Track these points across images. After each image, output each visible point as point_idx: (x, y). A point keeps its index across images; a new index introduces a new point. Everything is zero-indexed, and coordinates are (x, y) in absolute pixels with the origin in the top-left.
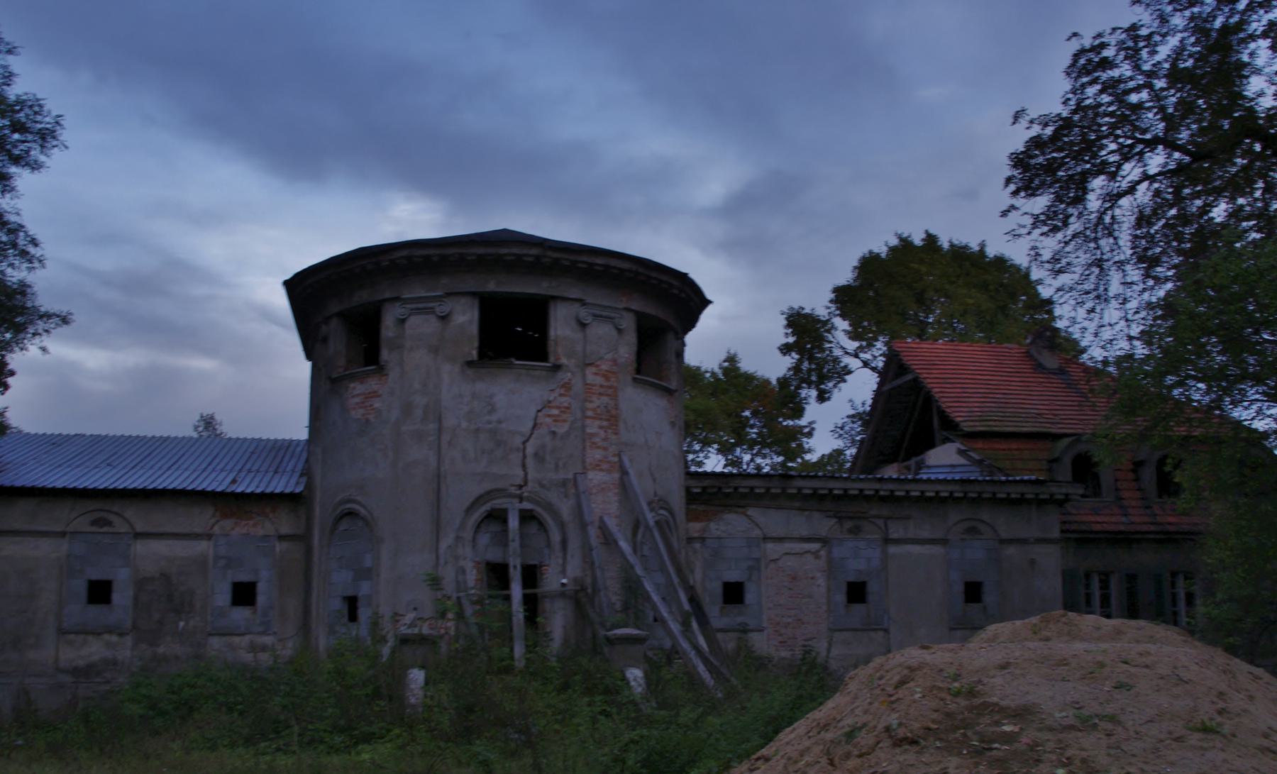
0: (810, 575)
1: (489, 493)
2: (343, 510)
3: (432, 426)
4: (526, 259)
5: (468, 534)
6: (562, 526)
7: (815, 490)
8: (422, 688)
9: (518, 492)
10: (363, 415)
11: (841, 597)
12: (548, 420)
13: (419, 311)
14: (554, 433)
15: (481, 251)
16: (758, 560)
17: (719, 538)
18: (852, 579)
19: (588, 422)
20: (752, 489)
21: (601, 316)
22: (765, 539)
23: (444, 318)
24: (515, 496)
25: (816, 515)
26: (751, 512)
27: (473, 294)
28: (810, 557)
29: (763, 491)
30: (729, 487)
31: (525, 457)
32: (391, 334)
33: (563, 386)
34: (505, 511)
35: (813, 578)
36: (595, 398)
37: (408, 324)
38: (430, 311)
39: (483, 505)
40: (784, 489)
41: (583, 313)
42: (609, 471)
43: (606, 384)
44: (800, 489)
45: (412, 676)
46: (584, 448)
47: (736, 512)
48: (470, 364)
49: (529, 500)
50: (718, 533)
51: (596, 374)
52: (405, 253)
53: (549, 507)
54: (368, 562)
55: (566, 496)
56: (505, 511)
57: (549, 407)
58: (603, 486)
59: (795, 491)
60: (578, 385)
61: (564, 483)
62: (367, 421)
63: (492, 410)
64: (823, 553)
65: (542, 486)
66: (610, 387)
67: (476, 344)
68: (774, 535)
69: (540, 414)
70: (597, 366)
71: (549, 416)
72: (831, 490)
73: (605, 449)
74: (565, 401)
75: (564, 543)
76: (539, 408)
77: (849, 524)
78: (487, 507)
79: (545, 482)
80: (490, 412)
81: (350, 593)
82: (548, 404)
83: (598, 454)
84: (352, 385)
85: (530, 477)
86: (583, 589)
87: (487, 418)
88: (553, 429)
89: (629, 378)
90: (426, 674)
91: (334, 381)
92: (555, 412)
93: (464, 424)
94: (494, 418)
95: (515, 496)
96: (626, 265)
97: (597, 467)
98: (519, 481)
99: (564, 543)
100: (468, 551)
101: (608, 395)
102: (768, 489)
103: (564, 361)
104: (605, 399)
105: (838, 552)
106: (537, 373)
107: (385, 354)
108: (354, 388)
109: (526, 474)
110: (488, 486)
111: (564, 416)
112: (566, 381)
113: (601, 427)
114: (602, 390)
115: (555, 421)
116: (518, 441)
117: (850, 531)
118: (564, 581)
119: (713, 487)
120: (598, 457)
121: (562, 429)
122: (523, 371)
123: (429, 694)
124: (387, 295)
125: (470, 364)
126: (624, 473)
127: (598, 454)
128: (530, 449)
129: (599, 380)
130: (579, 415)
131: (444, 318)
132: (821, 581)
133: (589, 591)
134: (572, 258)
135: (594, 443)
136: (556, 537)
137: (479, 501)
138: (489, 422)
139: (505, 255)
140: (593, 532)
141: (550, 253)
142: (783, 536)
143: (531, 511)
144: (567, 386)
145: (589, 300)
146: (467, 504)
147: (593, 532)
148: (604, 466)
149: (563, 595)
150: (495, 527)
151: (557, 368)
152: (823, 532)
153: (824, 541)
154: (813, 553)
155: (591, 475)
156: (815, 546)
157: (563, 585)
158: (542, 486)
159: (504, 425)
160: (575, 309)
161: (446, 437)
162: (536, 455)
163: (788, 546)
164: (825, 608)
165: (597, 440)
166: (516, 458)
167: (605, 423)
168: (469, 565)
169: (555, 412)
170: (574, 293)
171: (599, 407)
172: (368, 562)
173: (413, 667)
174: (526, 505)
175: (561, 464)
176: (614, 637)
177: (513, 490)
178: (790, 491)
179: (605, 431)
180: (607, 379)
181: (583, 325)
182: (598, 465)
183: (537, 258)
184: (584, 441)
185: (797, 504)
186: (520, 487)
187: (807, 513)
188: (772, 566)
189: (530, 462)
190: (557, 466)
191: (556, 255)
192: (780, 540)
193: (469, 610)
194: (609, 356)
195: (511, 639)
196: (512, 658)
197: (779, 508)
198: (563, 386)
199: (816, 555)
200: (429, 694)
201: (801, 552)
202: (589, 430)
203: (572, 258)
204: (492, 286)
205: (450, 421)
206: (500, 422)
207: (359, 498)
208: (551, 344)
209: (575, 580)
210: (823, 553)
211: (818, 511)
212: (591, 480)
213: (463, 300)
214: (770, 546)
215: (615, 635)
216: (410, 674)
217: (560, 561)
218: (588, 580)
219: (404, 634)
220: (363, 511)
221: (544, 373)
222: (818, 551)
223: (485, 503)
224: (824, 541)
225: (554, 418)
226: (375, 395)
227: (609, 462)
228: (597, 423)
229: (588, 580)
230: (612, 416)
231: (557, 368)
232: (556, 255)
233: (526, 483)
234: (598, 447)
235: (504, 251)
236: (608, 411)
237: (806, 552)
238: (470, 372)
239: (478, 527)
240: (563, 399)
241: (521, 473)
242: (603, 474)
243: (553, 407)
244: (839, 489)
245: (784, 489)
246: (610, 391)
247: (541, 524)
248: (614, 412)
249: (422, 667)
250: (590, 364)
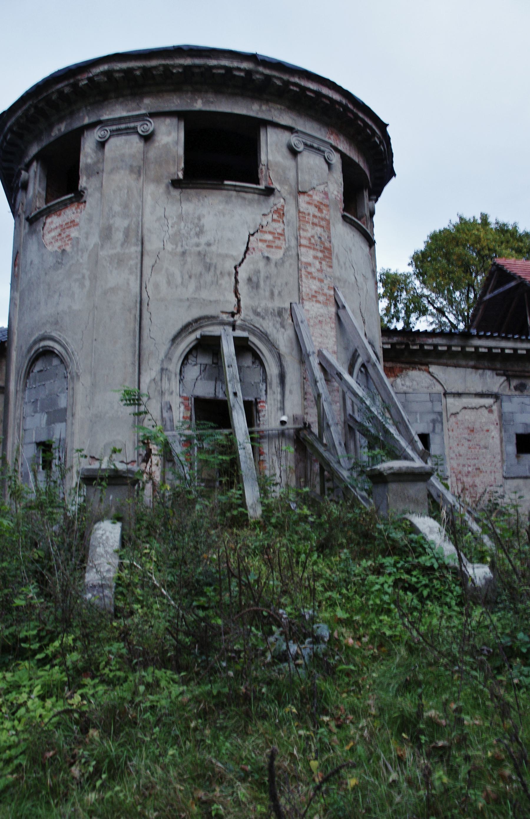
0: (485, 428)
1: (196, 321)
2: (39, 349)
3: (135, 249)
4: (237, 73)
5: (175, 366)
6: (279, 357)
7: (490, 349)
8: (117, 552)
9: (231, 319)
10: (59, 248)
11: (512, 448)
12: (260, 244)
13: (118, 133)
14: (268, 258)
15: (188, 62)
16: (440, 414)
17: (405, 393)
18: (521, 431)
19: (303, 250)
20: (436, 346)
21: (312, 147)
22: (445, 394)
23: (148, 138)
24: (228, 324)
25: (489, 373)
26: (433, 369)
27: (179, 115)
28: (485, 412)
29: (445, 348)
30: (415, 344)
31: (237, 281)
32: (89, 161)
33: (276, 211)
34: (218, 339)
35: (488, 431)
36: (309, 227)
37: (107, 146)
38: (134, 130)
39: (190, 333)
40: (463, 348)
41: (294, 140)
42: (325, 304)
43: (318, 214)
44: (477, 348)
45: (100, 532)
46: (300, 277)
47: (420, 369)
48: (176, 184)
49: (243, 329)
50: (405, 388)
51: (309, 203)
52: (105, 67)
53: (265, 337)
54: (62, 403)
55: (283, 326)
56: (218, 339)
57: (261, 231)
58: (320, 318)
59: (473, 350)
60: (291, 211)
61: (280, 313)
62: (64, 251)
63: (200, 232)
64: (495, 408)
65: (258, 314)
66: (323, 219)
67: (182, 165)
68: (453, 391)
69: (252, 238)
70: (310, 196)
71: (261, 240)
72: (503, 349)
73: (321, 281)
74: (278, 227)
75: (282, 377)
76: (252, 232)
77: (515, 382)
78: (197, 334)
79: (259, 310)
80: (198, 235)
81: (43, 438)
82: (260, 229)
83: (314, 285)
84: (49, 220)
85: (242, 304)
86: (307, 427)
87: (195, 240)
88: (266, 254)
89: (339, 216)
90: (123, 529)
91: (32, 221)
92: (269, 237)
93: (169, 247)
94: (203, 240)
95: (228, 324)
96: (336, 97)
97: (313, 297)
98: (232, 308)
99: (282, 377)
100: (175, 385)
101: (322, 227)
102: (449, 347)
103: (276, 185)
104: (319, 230)
105: (507, 407)
106: (249, 196)
107: (83, 182)
108: (52, 222)
109: (239, 301)
110: (196, 313)
111: (278, 243)
112: (279, 206)
113: (315, 257)
114: (316, 221)
115: (268, 246)
116: (229, 265)
117: (516, 388)
118: (284, 418)
119: (401, 343)
120: (314, 288)
121: (276, 255)
122: (234, 193)
123: (127, 562)
124: (87, 121)
125: (176, 184)
126: (339, 306)
127: (314, 285)
128: (243, 275)
129: (313, 210)
130: (293, 243)
131: (148, 138)
132: (495, 433)
133: (315, 429)
134: (285, 77)
135: (310, 273)
136: (273, 370)
137: (186, 329)
138: (198, 245)
139: (215, 67)
140: (314, 361)
141: (261, 69)
142: (460, 391)
143: (247, 339)
144: (280, 213)
145: (299, 127)
146: (171, 336)
147: (314, 361)
148: (321, 298)
149: (282, 434)
150: (205, 360)
151: (269, 192)
152: (495, 389)
153: (496, 397)
154: (486, 408)
155: (308, 305)
156: (489, 401)
157: (283, 423)
158: (258, 314)
159: (214, 248)
160: (285, 137)
161: (148, 262)
162: (250, 280)
163: (466, 401)
164: (499, 457)
165: (312, 269)
166: (228, 283)
167: (320, 255)
168: (176, 401)
169: (269, 237)
170: (286, 119)
171: (313, 237)
172: (62, 403)
173: (100, 519)
174: (239, 333)
175: (276, 292)
176: (389, 472)
177: (225, 317)
178: (468, 349)
179: (320, 263)
180: (320, 210)
181: (294, 152)
182: (314, 296)
183: (248, 72)
184: (299, 270)
185: (472, 363)
186: (233, 314)
187: (480, 371)
188: (453, 419)
189: (243, 288)
190: (272, 294)
191: (267, 72)
192: (459, 395)
193: (178, 449)
194: (321, 188)
195: (240, 480)
196: (244, 505)
197: (456, 366)
198: (276, 211)
199: (490, 410)
200: (127, 562)
201: (477, 407)
202: (303, 259)
203: (285, 77)
204: (199, 105)
205: (152, 245)
206: (209, 244)
207: (53, 334)
208: (262, 168)
209: (295, 419)
210: (495, 408)
211: (489, 369)
212: (308, 311)
213: (168, 121)
214: (450, 400)
215: (391, 468)
216: (98, 529)
217: (279, 397)
218: (312, 419)
219: (88, 470)
220: (58, 348)
221: (256, 196)
222: (491, 406)
223: (194, 331)
224: (496, 397)
225: (267, 243)
226: (73, 224)
227: (325, 295)
228: (311, 252)
229: (312, 419)
230: (325, 248)
231: (269, 192)
232: (267, 72)
233: (239, 311)
234: (314, 278)
235: (213, 62)
236: (322, 243)
237: (481, 407)
238: (176, 193)
239: (186, 358)
240: (275, 225)
241: (234, 300)
242: (318, 305)
243: (265, 232)
244: (510, 349)
245: (463, 348)
246: (323, 223)
247: (257, 358)
248: (327, 245)
249: (118, 519)
250: (304, 193)
